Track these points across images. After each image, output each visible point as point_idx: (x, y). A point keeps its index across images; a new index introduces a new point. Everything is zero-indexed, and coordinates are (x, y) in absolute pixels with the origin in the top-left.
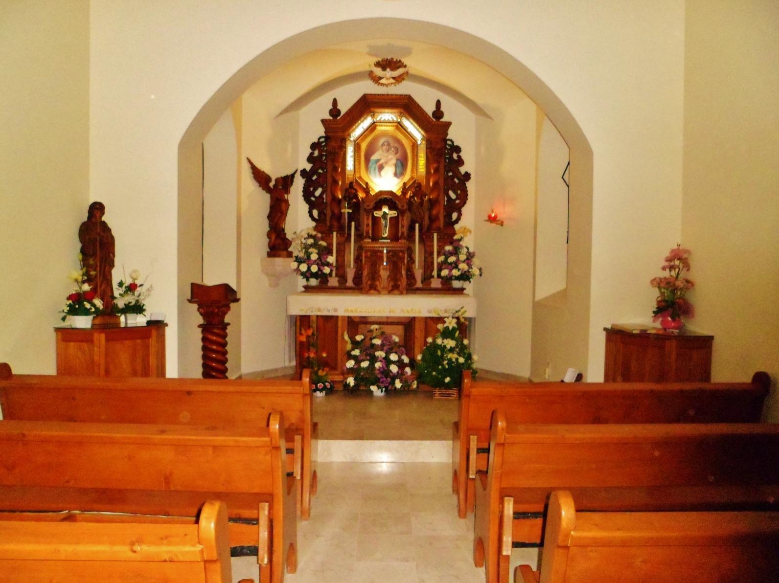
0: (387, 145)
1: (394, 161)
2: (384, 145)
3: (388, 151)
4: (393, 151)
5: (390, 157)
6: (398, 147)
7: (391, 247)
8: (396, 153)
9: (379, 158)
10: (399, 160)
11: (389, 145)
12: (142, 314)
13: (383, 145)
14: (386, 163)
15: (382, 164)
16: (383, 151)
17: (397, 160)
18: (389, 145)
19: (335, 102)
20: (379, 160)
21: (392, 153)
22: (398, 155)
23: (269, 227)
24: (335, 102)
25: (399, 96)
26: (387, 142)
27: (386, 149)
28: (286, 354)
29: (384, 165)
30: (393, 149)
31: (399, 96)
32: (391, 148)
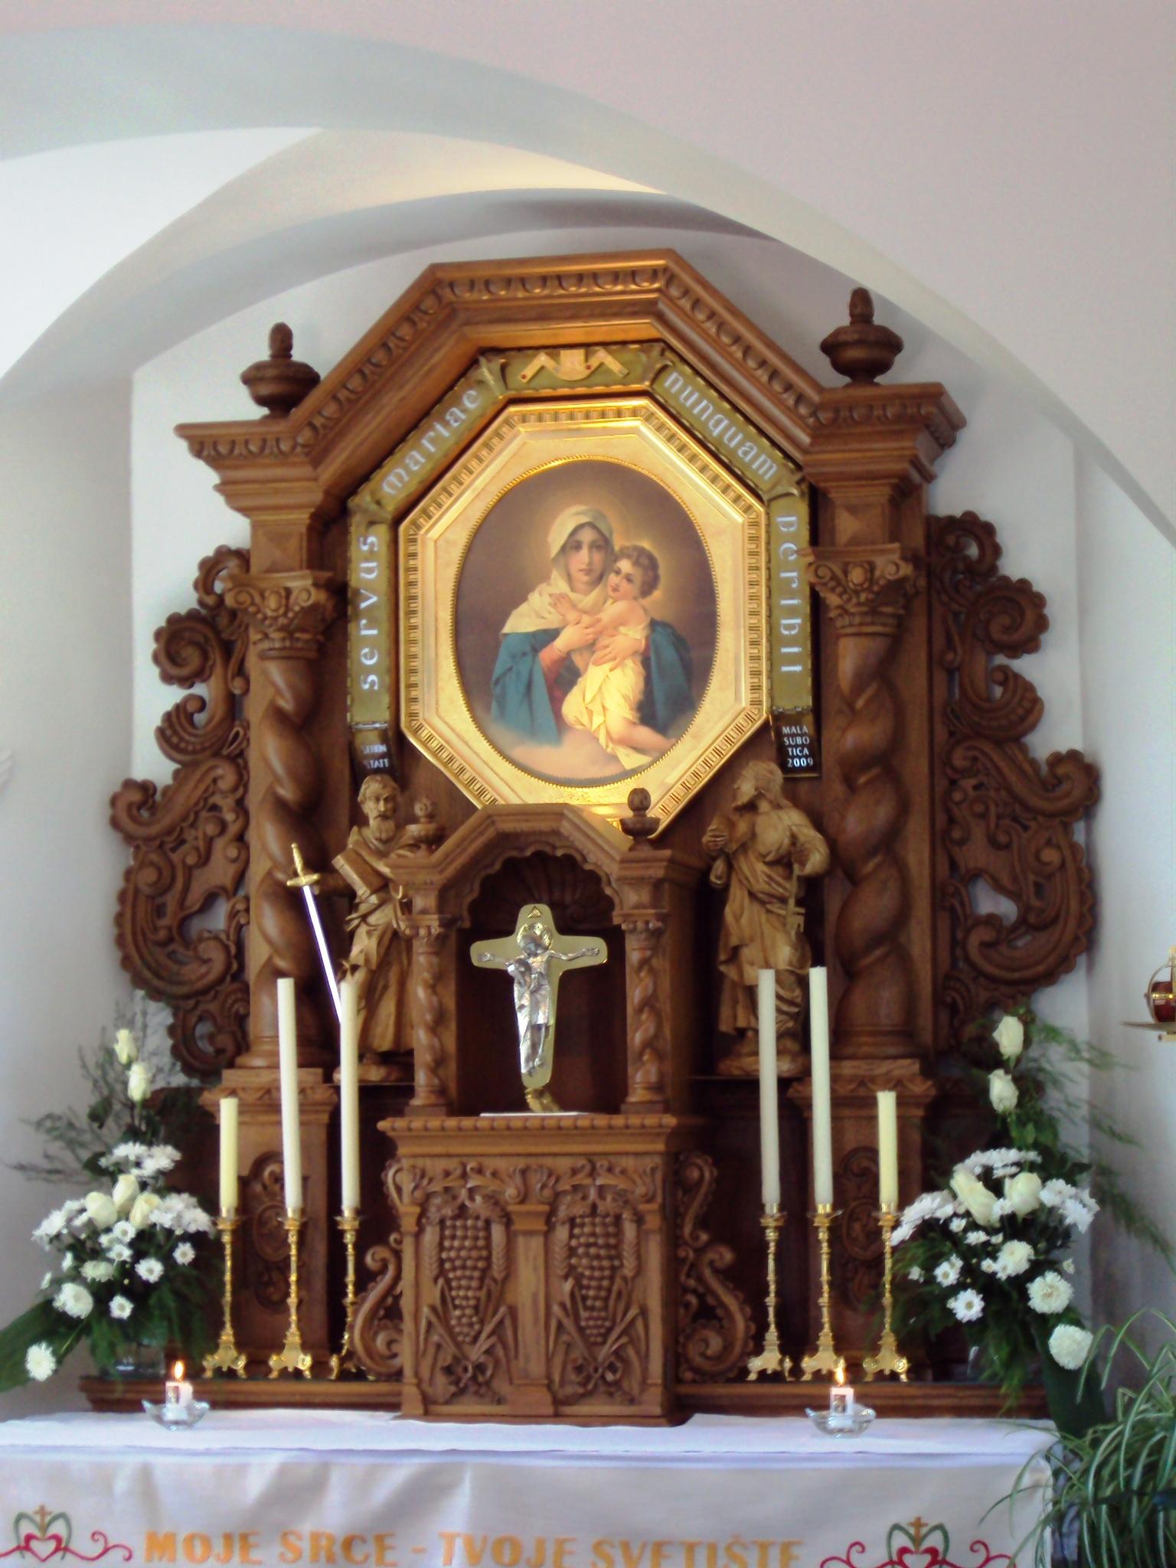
0: (594, 546)
1: (634, 635)
2: (578, 546)
3: (598, 579)
4: (629, 578)
5: (613, 609)
6: (656, 554)
7: (885, 1397)
8: (648, 588)
9: (551, 621)
10: (665, 625)
11: (603, 544)
12: (173, 1060)
13: (572, 545)
14: (591, 646)
15: (568, 655)
16: (569, 578)
17: (653, 624)
18: (603, 544)
19: (282, 338)
20: (551, 635)
21: (625, 586)
22: (657, 594)
23: (1024, 586)
24: (282, 338)
25: (268, 1033)
26: (592, 525)
27: (588, 571)
28: (433, 597)
29: (578, 660)
30: (625, 565)
31: (268, 1033)
32: (616, 559)
